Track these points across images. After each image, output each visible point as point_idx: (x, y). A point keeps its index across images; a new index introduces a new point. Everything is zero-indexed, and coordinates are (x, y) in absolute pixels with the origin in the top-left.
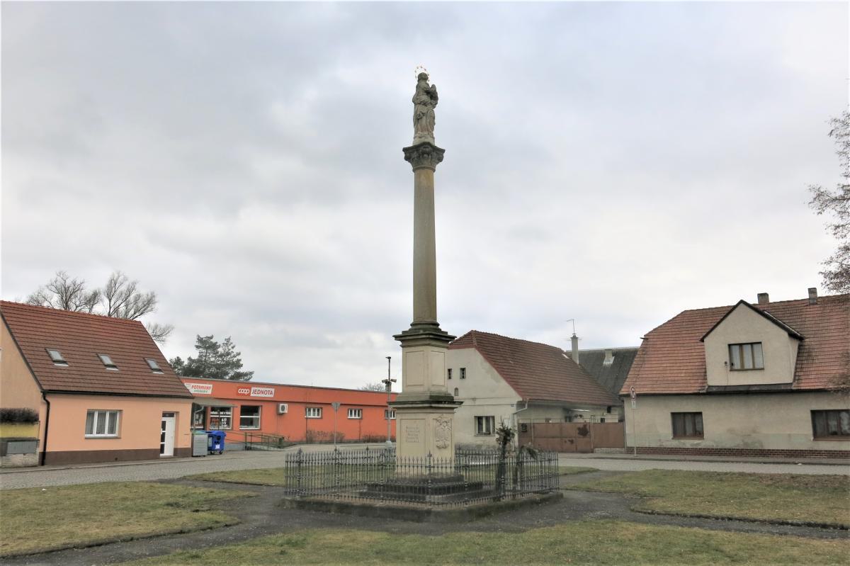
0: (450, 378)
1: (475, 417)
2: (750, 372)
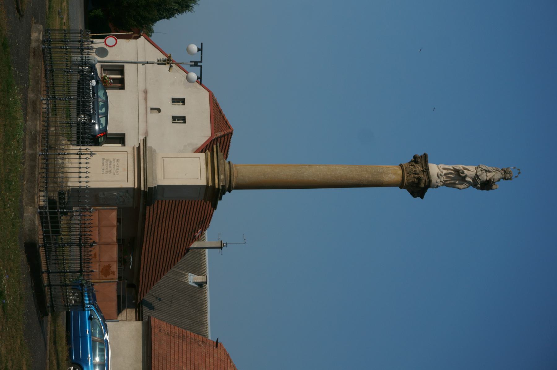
0: (202, 44)
1: (124, 135)
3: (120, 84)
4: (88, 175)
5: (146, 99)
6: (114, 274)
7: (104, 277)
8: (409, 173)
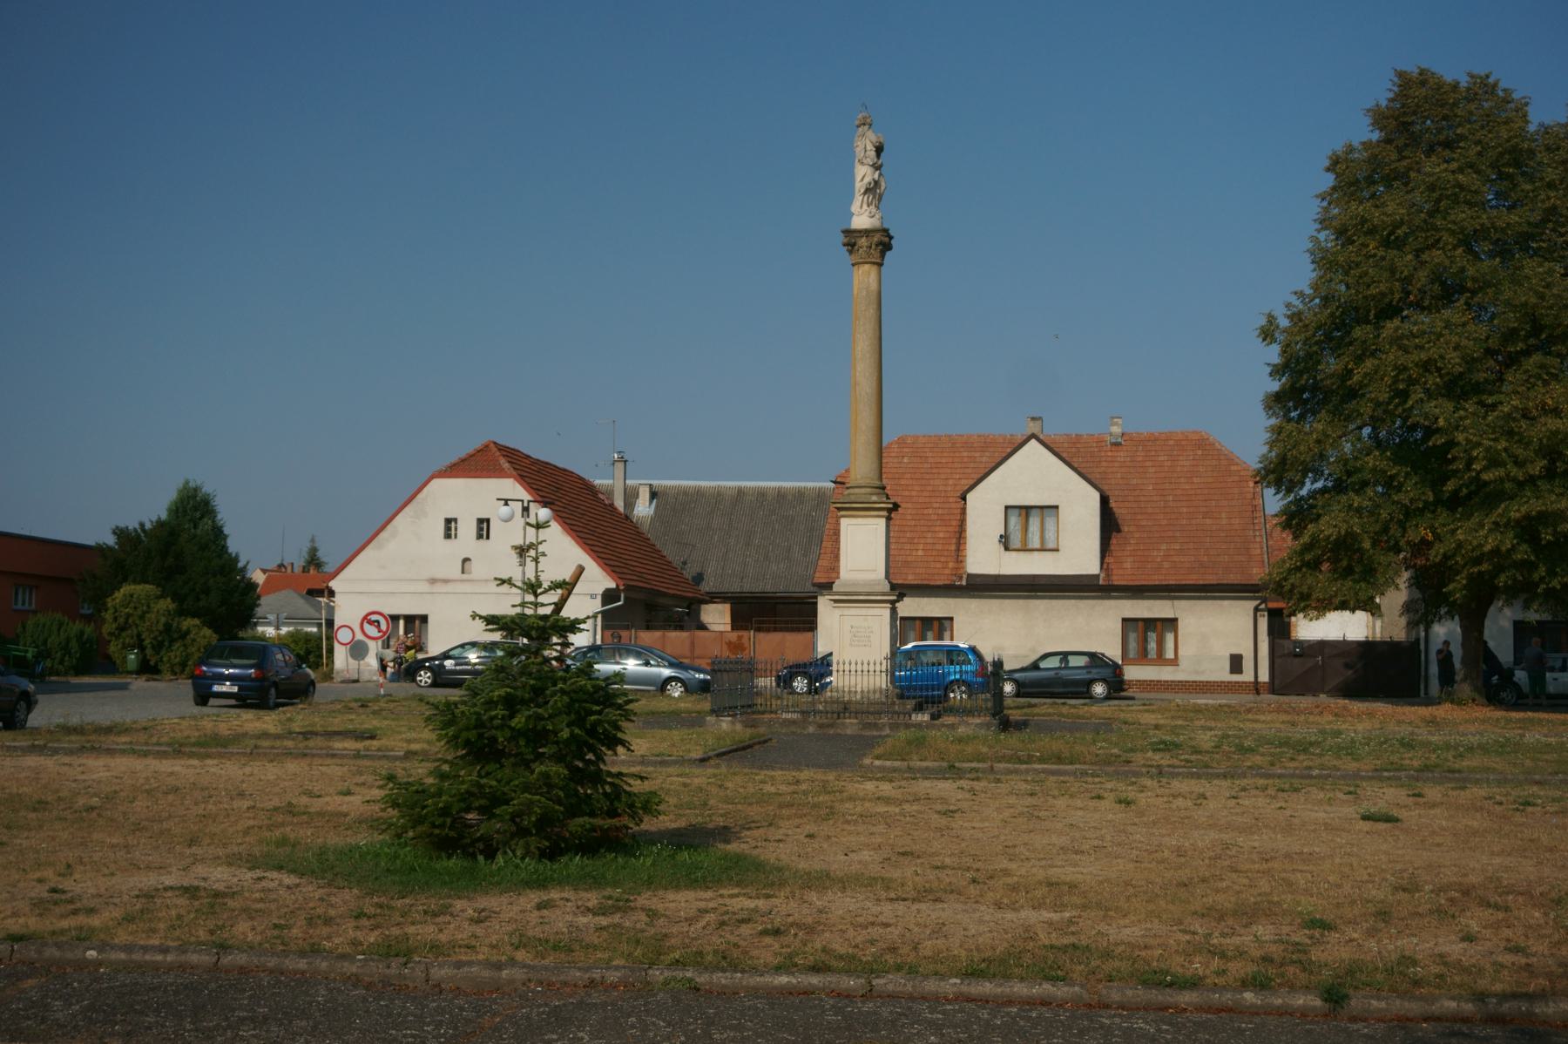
2: (1036, 553)
3: (417, 622)
4: (865, 662)
5: (446, 581)
6: (742, 636)
7: (747, 651)
8: (869, 255)
